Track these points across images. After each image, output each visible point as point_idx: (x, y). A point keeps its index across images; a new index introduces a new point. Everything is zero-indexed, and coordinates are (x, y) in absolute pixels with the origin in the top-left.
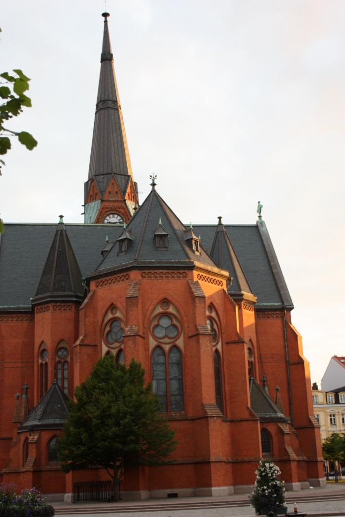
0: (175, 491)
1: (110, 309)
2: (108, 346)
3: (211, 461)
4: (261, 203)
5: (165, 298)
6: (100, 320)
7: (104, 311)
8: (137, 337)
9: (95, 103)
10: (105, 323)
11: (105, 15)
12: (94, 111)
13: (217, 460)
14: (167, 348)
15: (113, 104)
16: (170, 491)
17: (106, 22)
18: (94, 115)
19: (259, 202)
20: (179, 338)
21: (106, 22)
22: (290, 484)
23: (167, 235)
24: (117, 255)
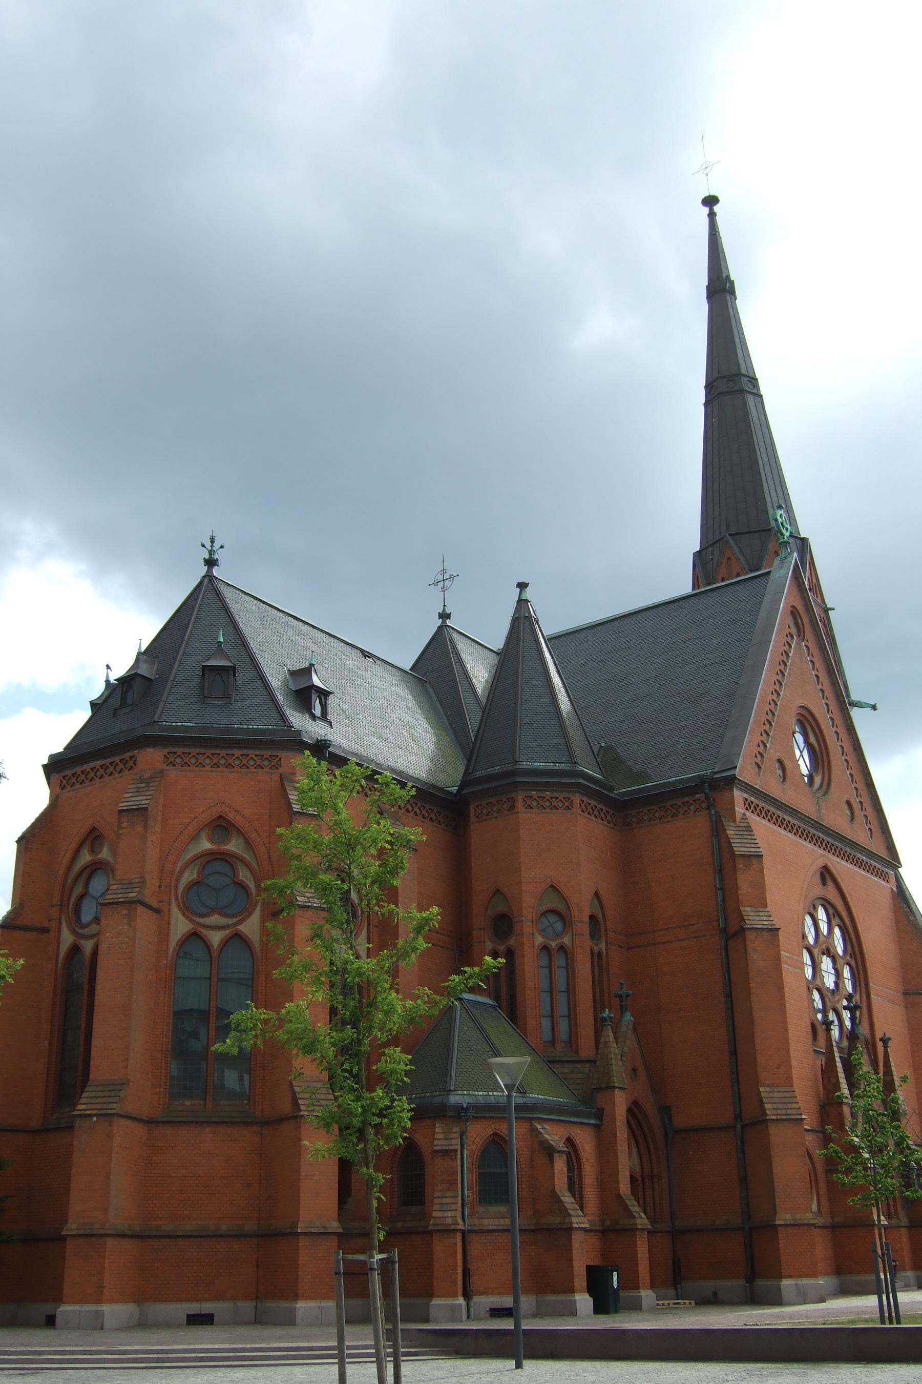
0: (206, 1307)
1: (88, 843)
2: (73, 931)
3: (777, 1223)
4: (528, 594)
5: (221, 817)
6: (62, 871)
7: (74, 845)
8: (140, 909)
9: (703, 382)
10: (70, 881)
11: (710, 201)
12: (702, 399)
13: (82, 1232)
14: (216, 938)
15: (749, 385)
16: (196, 1308)
17: (712, 215)
18: (702, 410)
19: (522, 586)
20: (250, 914)
21: (712, 215)
22: (284, 1304)
23: (234, 668)
24: (114, 715)
